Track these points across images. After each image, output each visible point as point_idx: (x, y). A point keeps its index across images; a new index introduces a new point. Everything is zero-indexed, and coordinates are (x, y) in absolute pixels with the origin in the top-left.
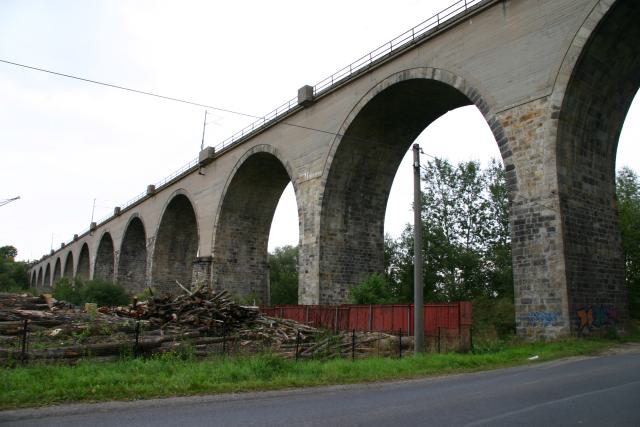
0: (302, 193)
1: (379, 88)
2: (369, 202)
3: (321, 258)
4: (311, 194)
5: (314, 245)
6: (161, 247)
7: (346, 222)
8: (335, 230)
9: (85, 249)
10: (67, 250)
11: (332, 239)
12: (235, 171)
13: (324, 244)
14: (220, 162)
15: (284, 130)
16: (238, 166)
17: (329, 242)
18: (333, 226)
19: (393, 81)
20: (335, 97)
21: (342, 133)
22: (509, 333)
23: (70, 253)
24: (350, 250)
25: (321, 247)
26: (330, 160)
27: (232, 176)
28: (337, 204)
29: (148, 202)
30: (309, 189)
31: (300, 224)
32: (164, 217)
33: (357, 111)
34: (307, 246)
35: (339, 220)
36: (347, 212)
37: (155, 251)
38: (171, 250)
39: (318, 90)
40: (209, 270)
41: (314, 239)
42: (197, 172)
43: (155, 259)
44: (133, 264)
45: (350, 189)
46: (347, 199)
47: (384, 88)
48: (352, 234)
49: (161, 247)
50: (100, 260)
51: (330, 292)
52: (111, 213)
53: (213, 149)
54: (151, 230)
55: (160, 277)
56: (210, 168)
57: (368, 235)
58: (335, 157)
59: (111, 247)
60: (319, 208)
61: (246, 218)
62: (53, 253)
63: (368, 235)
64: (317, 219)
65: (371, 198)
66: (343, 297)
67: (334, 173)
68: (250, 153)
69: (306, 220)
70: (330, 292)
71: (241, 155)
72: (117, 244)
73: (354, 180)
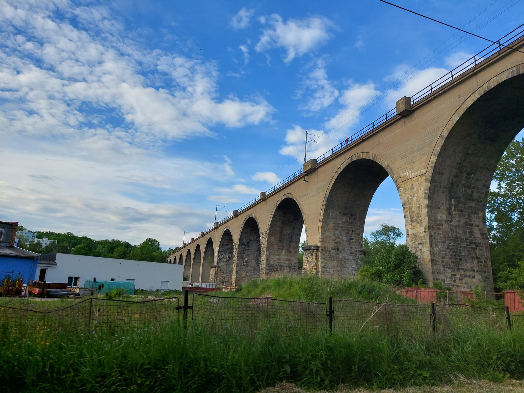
0: (405, 190)
1: (486, 87)
2: (471, 196)
3: (431, 246)
4: (415, 190)
5: (423, 234)
6: (272, 239)
7: (450, 214)
8: (441, 221)
9: (210, 243)
10: (196, 243)
11: (439, 229)
12: (336, 176)
13: (432, 233)
14: (320, 170)
15: (384, 137)
16: (339, 172)
17: (437, 231)
18: (439, 217)
19: (504, 77)
20: (434, 103)
21: (446, 134)
22: (99, 294)
23: (198, 246)
24: (456, 239)
25: (431, 236)
26: (434, 159)
27: (334, 180)
28: (442, 198)
29: (259, 205)
30: (413, 185)
31: (405, 216)
32: (274, 216)
33: (461, 112)
34: (415, 235)
35: (444, 212)
36: (451, 205)
37: (268, 242)
38: (280, 241)
39: (267, 193)
40: (317, 256)
41: (423, 229)
42: (303, 179)
43: (268, 248)
44: (248, 253)
45: (452, 184)
46: (450, 193)
47: (492, 86)
48: (457, 224)
49: (272, 239)
50: (222, 250)
51: (442, 277)
52: (231, 214)
53: (316, 160)
54: (264, 226)
55: (272, 263)
56: (313, 178)
57: (472, 225)
58: (439, 156)
59: (231, 240)
60: (426, 202)
61: (344, 214)
62: (185, 246)
63: (472, 225)
64: (424, 211)
65: (472, 192)
66: (455, 281)
67: (438, 170)
68: (349, 161)
69: (412, 212)
70: (442, 277)
71: (341, 163)
72: (236, 238)
73: (456, 176)
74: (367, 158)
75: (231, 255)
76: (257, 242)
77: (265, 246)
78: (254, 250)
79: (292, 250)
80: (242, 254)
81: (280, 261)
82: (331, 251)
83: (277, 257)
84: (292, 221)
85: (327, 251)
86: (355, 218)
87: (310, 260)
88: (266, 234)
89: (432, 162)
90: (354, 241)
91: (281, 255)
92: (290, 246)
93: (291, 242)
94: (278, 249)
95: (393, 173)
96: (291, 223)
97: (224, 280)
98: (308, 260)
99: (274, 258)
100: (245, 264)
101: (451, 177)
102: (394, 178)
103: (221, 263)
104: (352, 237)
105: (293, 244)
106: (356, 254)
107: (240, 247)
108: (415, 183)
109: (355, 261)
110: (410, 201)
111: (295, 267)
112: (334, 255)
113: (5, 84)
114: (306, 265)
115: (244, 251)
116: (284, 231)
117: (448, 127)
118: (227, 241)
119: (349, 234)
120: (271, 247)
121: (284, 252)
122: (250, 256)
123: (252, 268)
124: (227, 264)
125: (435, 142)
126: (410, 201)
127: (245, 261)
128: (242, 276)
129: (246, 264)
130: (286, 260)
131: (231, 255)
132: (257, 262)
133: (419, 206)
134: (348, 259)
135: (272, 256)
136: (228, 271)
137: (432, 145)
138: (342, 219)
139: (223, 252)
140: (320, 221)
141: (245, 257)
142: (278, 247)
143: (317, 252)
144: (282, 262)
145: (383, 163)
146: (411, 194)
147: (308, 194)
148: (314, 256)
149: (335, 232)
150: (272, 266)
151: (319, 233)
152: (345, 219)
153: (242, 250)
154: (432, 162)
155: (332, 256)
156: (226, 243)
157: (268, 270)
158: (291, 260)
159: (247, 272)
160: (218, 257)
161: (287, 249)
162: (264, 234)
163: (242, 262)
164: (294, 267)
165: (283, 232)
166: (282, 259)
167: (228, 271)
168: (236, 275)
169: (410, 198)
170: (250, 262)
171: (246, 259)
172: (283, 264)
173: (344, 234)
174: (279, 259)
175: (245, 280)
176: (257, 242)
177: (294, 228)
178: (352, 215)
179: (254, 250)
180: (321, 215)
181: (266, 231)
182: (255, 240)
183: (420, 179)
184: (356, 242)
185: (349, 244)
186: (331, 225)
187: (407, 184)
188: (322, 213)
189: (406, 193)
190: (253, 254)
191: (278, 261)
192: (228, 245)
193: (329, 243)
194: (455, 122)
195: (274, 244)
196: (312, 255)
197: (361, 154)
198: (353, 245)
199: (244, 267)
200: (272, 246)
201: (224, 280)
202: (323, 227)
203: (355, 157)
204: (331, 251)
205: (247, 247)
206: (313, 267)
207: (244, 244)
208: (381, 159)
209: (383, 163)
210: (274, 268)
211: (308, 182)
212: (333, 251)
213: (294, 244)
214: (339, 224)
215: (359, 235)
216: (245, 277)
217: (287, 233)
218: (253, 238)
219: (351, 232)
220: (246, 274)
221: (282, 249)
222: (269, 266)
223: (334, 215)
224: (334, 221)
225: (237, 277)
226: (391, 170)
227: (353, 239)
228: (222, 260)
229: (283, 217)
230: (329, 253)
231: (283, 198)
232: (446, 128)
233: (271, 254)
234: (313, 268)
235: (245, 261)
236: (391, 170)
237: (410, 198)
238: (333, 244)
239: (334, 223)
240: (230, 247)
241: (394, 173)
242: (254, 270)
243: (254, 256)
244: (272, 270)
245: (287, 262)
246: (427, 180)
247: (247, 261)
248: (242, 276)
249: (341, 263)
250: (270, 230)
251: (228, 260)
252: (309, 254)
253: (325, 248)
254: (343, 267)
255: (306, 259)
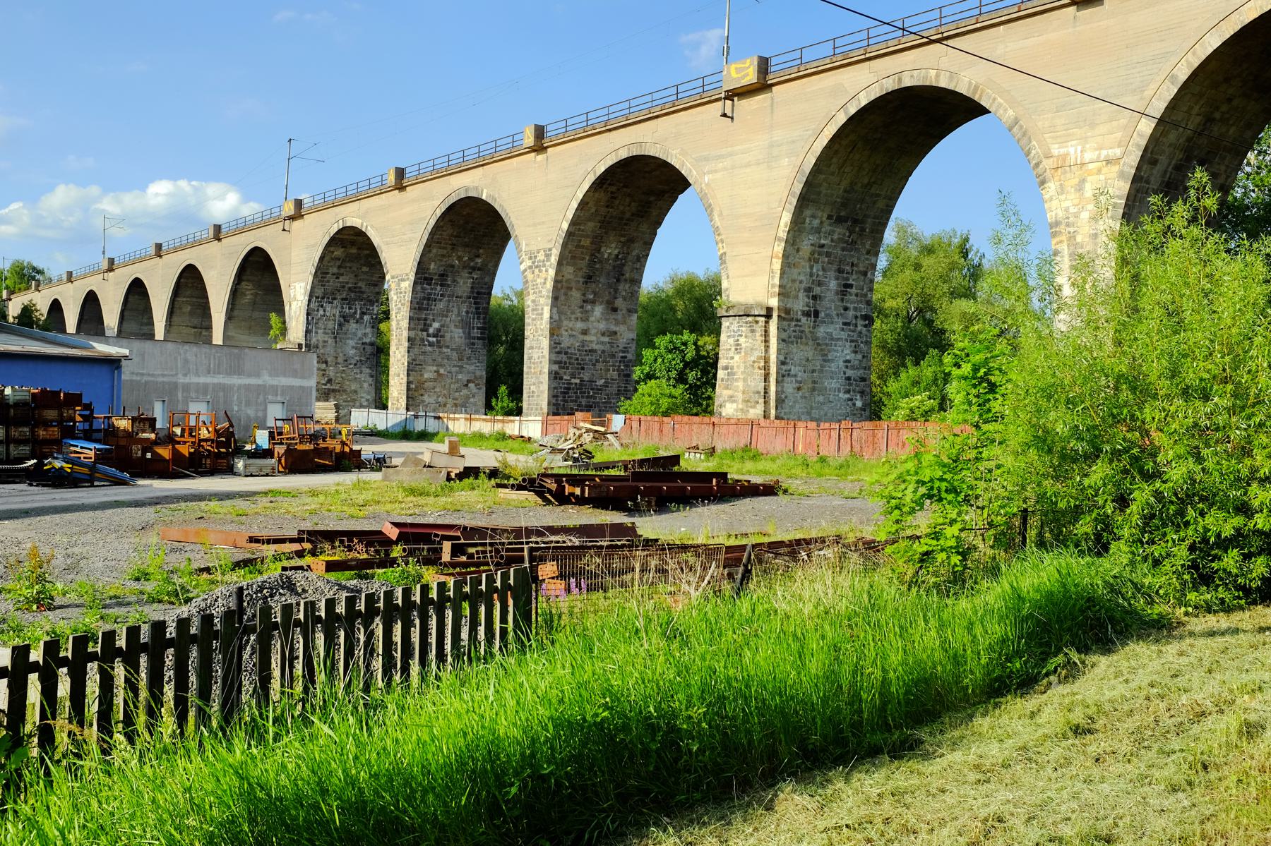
30: (1083, 181)
32: (583, 205)
38: (589, 279)
49: (569, 270)
50: (319, 292)
55: (566, 342)
61: (840, 220)
74: (951, 87)
75: (350, 308)
76: (470, 273)
77: (544, 293)
78: (461, 297)
79: (619, 303)
80: (425, 309)
81: (587, 338)
82: (800, 321)
83: (580, 325)
84: (628, 220)
85: (792, 320)
86: (863, 230)
87: (748, 344)
88: (548, 256)
89: (1140, 135)
90: (854, 290)
91: (592, 319)
92: (616, 292)
93: (618, 280)
94: (584, 301)
95: (1030, 142)
96: (626, 224)
97: (328, 386)
98: (738, 345)
99: (571, 329)
100: (431, 339)
101: (1170, 169)
102: (1032, 155)
103: (316, 333)
104: (851, 282)
105: (624, 287)
106: (856, 326)
107: (419, 288)
108: (1089, 178)
109: (853, 344)
110: (1071, 219)
111: (628, 352)
112: (807, 330)
113: (793, 142)
114: (732, 358)
115: (429, 299)
116: (602, 250)
117: (1190, 59)
118: (338, 263)
119: (843, 272)
120: (562, 298)
121: (598, 310)
122: (447, 317)
123: (455, 353)
124: (335, 338)
125: (1154, 86)
126: (1071, 219)
127: (431, 331)
128: (426, 376)
129: (434, 339)
130: (603, 334)
131: (350, 308)
132: (469, 333)
133: (1096, 234)
134: (838, 339)
135: (565, 323)
136: (340, 360)
137: (1146, 93)
138: (831, 233)
139: (323, 298)
140: (777, 239)
141: (434, 320)
142: (584, 295)
143: (767, 322)
144: (594, 338)
145: (1001, 112)
146: (1076, 202)
147: (731, 155)
148: (758, 334)
149: (811, 267)
150: (566, 353)
151: (772, 271)
152: (840, 231)
153: (424, 298)
154: (1140, 135)
155: (802, 332)
156: (335, 270)
157: (556, 362)
158: (615, 333)
159: (440, 365)
160: (308, 314)
161: (608, 302)
162: (541, 256)
163: (425, 333)
164: (624, 352)
165: (599, 251)
166: (593, 331)
167: (340, 360)
168: (408, 375)
169: (1072, 210)
170: (448, 336)
171: (436, 325)
172: (595, 346)
173: (832, 274)
174: (585, 332)
175: (434, 388)
176: (470, 273)
177: (631, 241)
178: (855, 221)
179: (461, 297)
180: (782, 224)
181: (550, 250)
182: (464, 267)
183: (1105, 170)
184: (857, 295)
185: (842, 300)
186: (806, 247)
187: (1068, 175)
188: (787, 218)
189: (1063, 197)
190: (455, 310)
191: (582, 337)
192: (342, 275)
193: (796, 297)
194: (1210, 50)
195: (571, 289)
196: (753, 331)
197: (933, 73)
198: (852, 303)
199: (429, 349)
200: (566, 294)
201: (328, 386)
202: (786, 256)
203: (912, 76)
204: (800, 321)
205: (439, 288)
206: (754, 362)
207: (432, 279)
208: (994, 99)
209: (1001, 112)
210: (571, 358)
211: (732, 118)
212: (804, 320)
213: (627, 286)
214: (823, 246)
215: (865, 274)
216: (435, 380)
217: (610, 254)
218: (460, 258)
219: (848, 268)
220: (437, 372)
221: (593, 302)
222: (559, 353)
223: (816, 222)
224: (813, 238)
225: (411, 379)
226: (1024, 134)
227: (851, 286)
228: (320, 325)
229: (607, 207)
230: (796, 326)
231: (624, 154)
232: (1187, 61)
233: (563, 318)
234: (756, 364)
235: (431, 331)
236: (1024, 134)
237: (1072, 210)
238: (806, 300)
239: (812, 245)
240: (347, 283)
241: (1034, 143)
242: (461, 360)
243: (459, 315)
244: (565, 363)
245: (606, 339)
246: (1122, 175)
247: (439, 330)
248: (426, 376)
249: (822, 350)
250: (564, 246)
251: (340, 325)
252: (744, 329)
253: (787, 311)
254: (825, 361)
255: (731, 341)
